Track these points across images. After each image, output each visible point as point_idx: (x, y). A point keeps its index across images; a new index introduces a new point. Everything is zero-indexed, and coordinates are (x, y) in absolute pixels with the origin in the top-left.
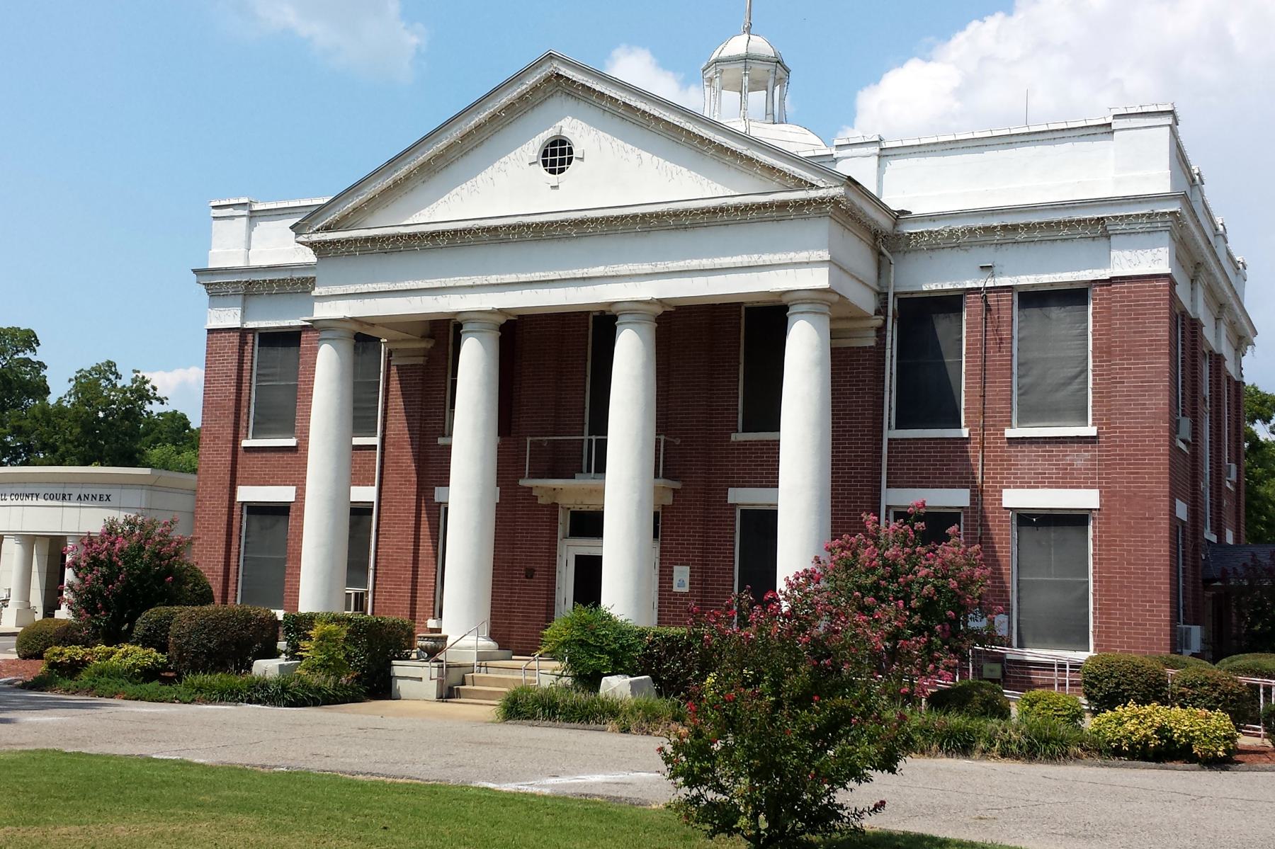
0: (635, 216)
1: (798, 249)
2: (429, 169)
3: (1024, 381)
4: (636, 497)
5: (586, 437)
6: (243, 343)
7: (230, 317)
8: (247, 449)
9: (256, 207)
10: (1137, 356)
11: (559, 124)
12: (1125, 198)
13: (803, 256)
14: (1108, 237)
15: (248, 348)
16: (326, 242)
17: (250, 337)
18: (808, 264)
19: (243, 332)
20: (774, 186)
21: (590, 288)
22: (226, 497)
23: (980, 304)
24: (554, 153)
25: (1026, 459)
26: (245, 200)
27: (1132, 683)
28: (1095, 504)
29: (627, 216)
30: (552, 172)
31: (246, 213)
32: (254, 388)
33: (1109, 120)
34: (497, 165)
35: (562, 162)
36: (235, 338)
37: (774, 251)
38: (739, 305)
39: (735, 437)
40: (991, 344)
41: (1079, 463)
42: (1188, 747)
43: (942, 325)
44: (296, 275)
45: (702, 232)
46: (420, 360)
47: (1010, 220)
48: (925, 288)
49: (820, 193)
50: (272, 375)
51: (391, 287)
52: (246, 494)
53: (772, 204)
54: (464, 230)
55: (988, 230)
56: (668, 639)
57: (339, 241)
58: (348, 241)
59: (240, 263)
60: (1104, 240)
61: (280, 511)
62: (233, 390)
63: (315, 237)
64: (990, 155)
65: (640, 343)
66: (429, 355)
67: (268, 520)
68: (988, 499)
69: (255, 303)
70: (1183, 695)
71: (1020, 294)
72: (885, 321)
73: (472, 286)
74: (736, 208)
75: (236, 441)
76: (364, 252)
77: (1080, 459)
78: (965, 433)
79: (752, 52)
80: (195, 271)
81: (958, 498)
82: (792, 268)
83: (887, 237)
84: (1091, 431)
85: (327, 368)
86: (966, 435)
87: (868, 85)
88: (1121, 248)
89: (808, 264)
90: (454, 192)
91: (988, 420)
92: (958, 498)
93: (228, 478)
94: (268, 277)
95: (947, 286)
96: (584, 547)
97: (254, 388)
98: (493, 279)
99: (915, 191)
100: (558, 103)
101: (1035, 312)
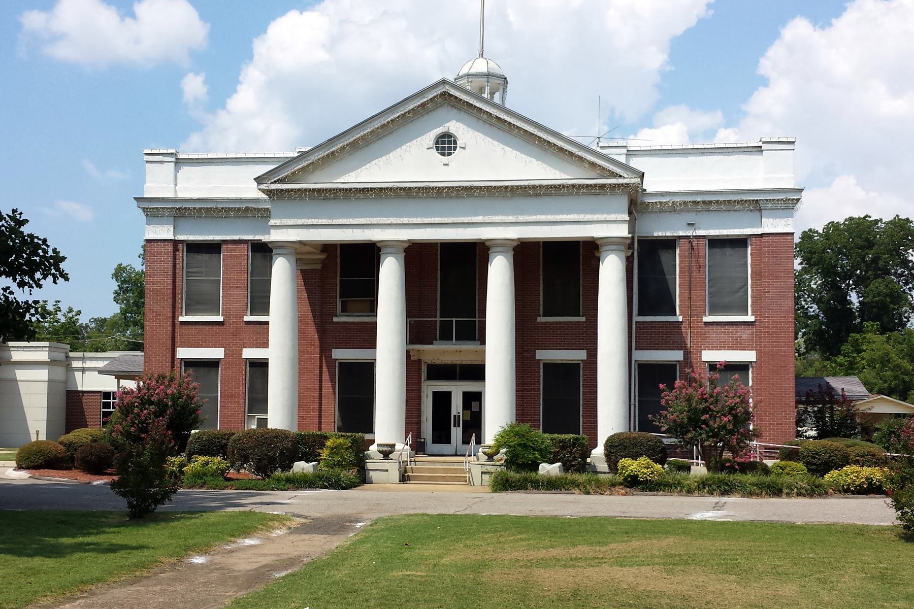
0: (506, 187)
1: (609, 213)
2: (355, 146)
3: (713, 289)
4: (509, 357)
5: (438, 319)
6: (175, 250)
7: (165, 232)
8: (183, 323)
9: (181, 156)
10: (777, 278)
11: (447, 125)
12: (772, 190)
13: (612, 217)
14: (760, 210)
15: (179, 254)
16: (282, 190)
17: (180, 246)
18: (615, 222)
19: (175, 243)
20: (593, 174)
21: (473, 229)
22: (169, 355)
23: (687, 245)
24: (443, 142)
25: (714, 333)
26: (173, 151)
27: (836, 456)
28: (681, 358)
29: (501, 187)
30: (443, 155)
31: (173, 159)
32: (185, 281)
33: (760, 144)
34: (404, 147)
35: (449, 149)
36: (170, 247)
37: (594, 213)
38: (579, 242)
39: (539, 319)
40: (694, 269)
41: (744, 336)
42: (880, 486)
43: (664, 256)
44: (220, 206)
45: (547, 199)
46: (319, 267)
47: (708, 198)
48: (655, 235)
49: (626, 181)
50: (202, 272)
51: (330, 222)
52: (183, 353)
53: (595, 185)
54: (387, 188)
55: (696, 203)
56: (560, 442)
57: (292, 190)
58: (299, 190)
59: (171, 195)
60: (757, 214)
61: (571, 369)
62: (170, 282)
63: (273, 187)
64: (691, 159)
65: (507, 264)
66: (323, 262)
67: (203, 371)
68: (693, 356)
69: (182, 222)
70: (858, 461)
71: (709, 240)
72: (633, 253)
73: (389, 224)
74: (573, 186)
75: (174, 318)
76: (312, 198)
77: (745, 334)
78: (680, 319)
79: (492, 71)
80: (135, 199)
81: (676, 356)
82: (609, 225)
83: (637, 203)
84: (750, 318)
85: (281, 273)
86: (681, 320)
87: (274, 19)
88: (768, 217)
89: (615, 222)
90: (373, 162)
91: (692, 311)
92: (676, 356)
93: (169, 342)
94: (198, 206)
95: (668, 234)
96: (471, 387)
97: (185, 281)
98: (405, 220)
99: (660, 179)
100: (444, 111)
101: (717, 251)
